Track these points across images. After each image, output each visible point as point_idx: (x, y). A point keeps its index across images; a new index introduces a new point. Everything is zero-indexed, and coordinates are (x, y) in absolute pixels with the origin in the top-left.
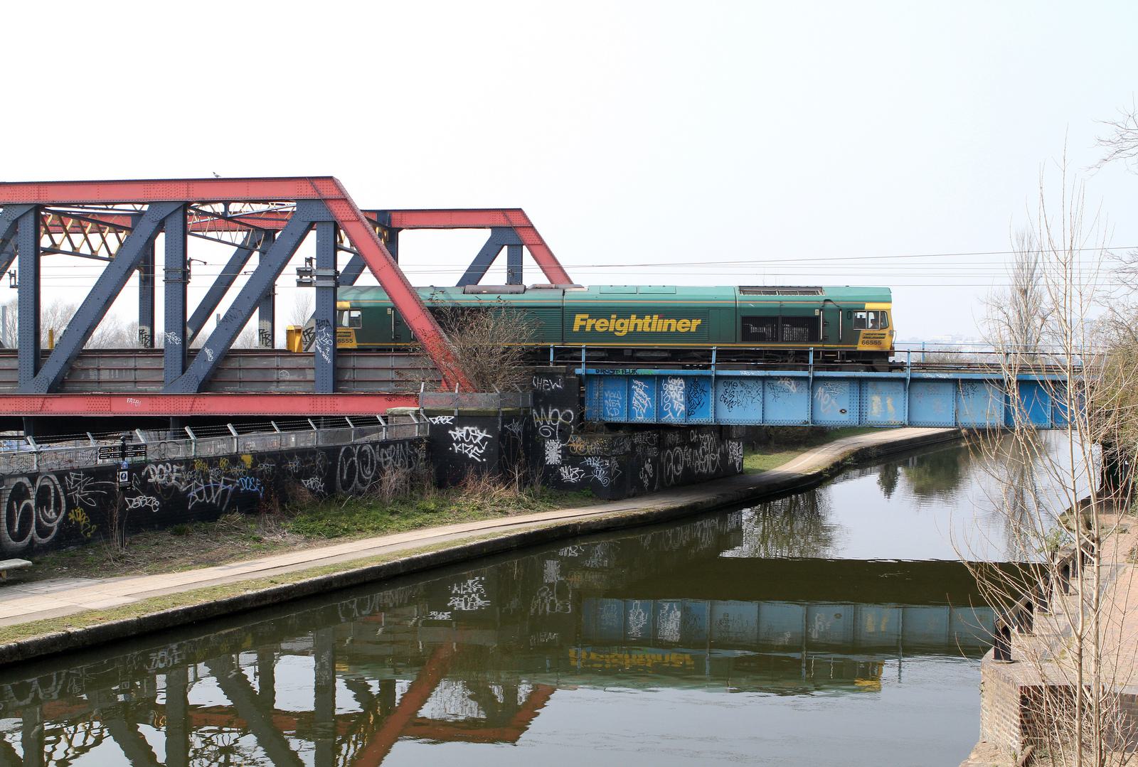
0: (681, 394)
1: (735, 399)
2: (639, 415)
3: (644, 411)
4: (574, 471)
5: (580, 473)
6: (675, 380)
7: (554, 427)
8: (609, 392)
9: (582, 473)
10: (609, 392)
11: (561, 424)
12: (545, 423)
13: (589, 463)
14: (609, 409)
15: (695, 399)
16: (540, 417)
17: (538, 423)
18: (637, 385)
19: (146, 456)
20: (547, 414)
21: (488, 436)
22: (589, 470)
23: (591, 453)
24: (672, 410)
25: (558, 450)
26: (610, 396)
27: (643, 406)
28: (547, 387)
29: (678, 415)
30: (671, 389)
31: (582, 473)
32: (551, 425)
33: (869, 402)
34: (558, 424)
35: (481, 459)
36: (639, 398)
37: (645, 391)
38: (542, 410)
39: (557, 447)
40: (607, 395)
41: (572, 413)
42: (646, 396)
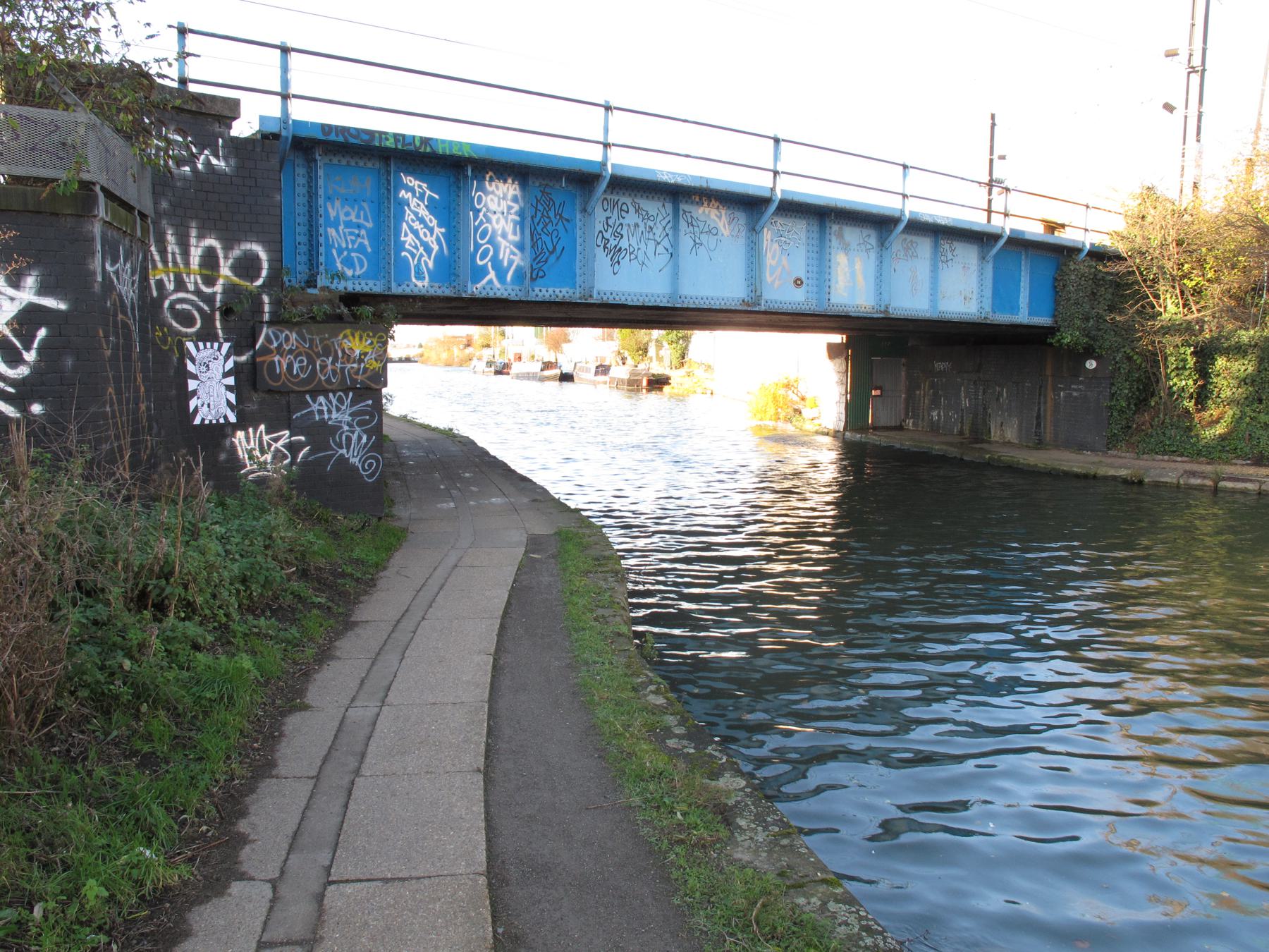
0: (513, 221)
1: (624, 244)
2: (419, 276)
3: (431, 264)
4: (276, 440)
5: (293, 448)
6: (501, 185)
7: (209, 299)
8: (337, 204)
9: (300, 446)
10: (337, 204)
11: (230, 289)
12: (180, 286)
13: (320, 412)
14: (340, 251)
15: (544, 236)
16: (165, 262)
17: (160, 284)
18: (412, 190)
19: (311, 639)
20: (186, 254)
21: (50, 302)
22: (321, 434)
23: (328, 381)
24: (496, 263)
25: (226, 375)
26: (342, 217)
27: (428, 250)
28: (180, 162)
29: (509, 277)
30: (493, 207)
31: (300, 446)
32: (198, 292)
33: (833, 264)
34: (218, 288)
35: (23, 407)
36: (417, 225)
37: (432, 207)
38: (171, 238)
39: (218, 368)
40: (332, 214)
41: (263, 255)
42: (435, 222)
